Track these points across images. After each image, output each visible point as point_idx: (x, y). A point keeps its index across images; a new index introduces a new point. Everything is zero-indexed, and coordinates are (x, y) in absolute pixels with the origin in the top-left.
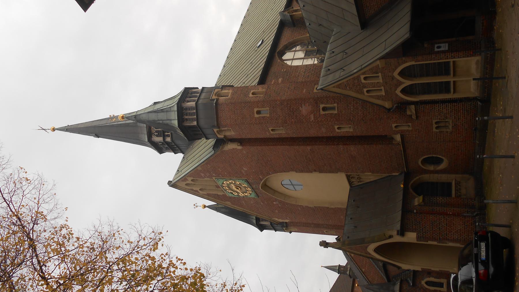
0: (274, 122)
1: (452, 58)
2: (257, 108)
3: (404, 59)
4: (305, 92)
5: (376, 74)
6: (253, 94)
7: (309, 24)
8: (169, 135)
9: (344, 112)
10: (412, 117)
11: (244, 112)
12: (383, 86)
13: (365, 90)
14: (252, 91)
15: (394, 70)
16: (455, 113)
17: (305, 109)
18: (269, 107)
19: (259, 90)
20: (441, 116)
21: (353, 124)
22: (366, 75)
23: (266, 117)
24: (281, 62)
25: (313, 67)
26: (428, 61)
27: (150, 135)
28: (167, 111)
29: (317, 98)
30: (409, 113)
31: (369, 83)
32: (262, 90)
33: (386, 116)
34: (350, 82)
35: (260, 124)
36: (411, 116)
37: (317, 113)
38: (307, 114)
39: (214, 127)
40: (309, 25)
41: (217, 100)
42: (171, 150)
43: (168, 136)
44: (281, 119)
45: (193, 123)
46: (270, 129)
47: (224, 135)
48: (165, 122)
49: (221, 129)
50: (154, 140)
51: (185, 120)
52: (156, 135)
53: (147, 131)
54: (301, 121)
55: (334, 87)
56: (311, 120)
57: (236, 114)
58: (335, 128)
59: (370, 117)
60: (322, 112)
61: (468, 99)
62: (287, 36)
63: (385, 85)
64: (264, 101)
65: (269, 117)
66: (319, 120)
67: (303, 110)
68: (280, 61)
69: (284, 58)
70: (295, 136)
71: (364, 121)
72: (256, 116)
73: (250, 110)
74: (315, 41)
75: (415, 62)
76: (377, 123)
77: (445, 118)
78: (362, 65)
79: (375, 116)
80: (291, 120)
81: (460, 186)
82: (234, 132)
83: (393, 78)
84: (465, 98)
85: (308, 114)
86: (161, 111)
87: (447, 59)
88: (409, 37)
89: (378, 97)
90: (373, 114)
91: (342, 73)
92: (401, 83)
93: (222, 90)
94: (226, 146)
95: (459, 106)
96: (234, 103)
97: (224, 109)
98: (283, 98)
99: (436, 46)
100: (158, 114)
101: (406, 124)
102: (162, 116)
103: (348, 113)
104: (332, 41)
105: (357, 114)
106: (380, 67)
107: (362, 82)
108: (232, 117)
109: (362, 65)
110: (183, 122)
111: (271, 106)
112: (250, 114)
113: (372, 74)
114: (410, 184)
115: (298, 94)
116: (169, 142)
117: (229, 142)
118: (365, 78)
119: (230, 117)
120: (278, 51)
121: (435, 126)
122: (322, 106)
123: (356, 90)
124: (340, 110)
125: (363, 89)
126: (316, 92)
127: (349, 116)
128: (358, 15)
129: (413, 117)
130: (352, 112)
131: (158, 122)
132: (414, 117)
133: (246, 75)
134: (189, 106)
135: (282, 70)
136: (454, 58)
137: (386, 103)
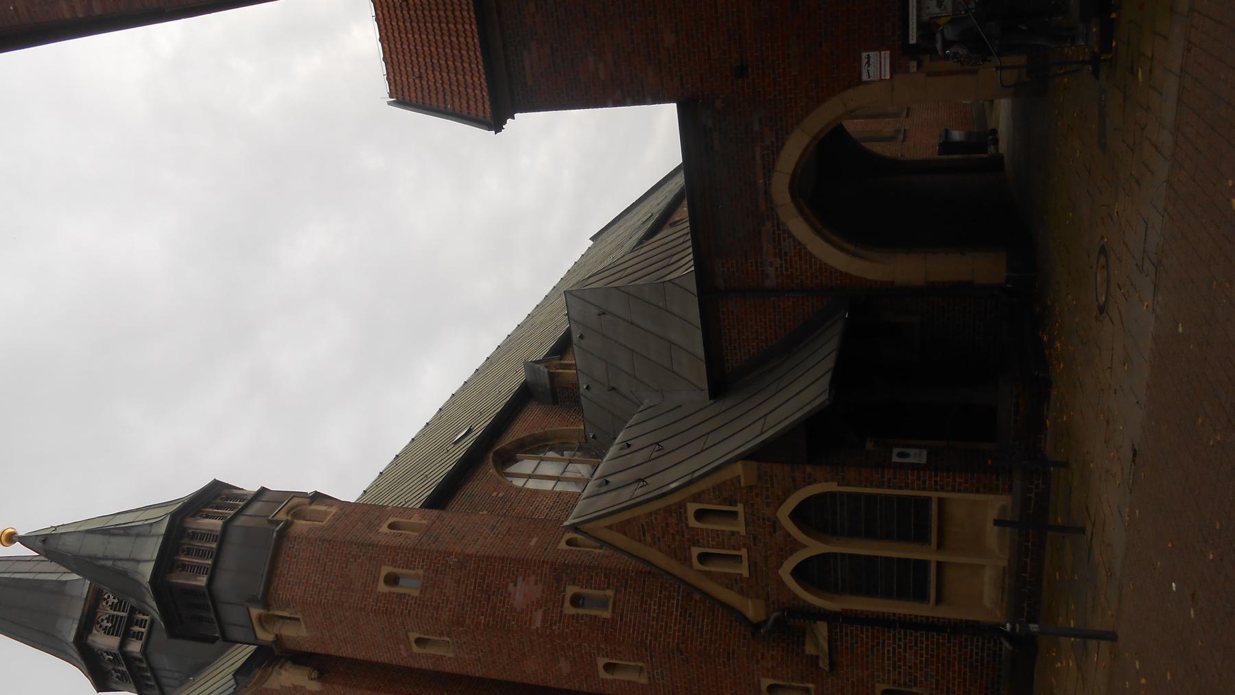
0: (427, 614)
1: (936, 490)
3: (809, 469)
4: (535, 546)
5: (731, 505)
6: (391, 526)
7: (588, 388)
8: (143, 633)
10: (817, 664)
11: (349, 571)
12: (744, 545)
13: (696, 551)
14: (391, 520)
15: (781, 501)
16: (938, 667)
17: (522, 592)
18: (424, 567)
19: (412, 520)
20: (900, 673)
21: (651, 658)
22: (701, 502)
23: (409, 595)
24: (496, 474)
26: (871, 487)
27: (88, 623)
28: (138, 535)
29: (564, 564)
30: (810, 649)
31: (707, 530)
32: (420, 522)
33: (746, 649)
34: (656, 519)
35: (386, 613)
36: (815, 659)
37: (553, 609)
38: (525, 607)
39: (253, 601)
40: (587, 391)
41: (288, 525)
42: (132, 685)
43: (138, 636)
44: (450, 611)
45: (196, 580)
46: (413, 636)
47: (276, 635)
48: (120, 564)
49: (271, 612)
50: (95, 642)
51: (178, 567)
52: (106, 627)
53: (83, 610)
54: (504, 626)
55: (610, 527)
57: (327, 575)
58: (597, 665)
60: (569, 610)
61: (974, 628)
62: (530, 423)
63: (752, 543)
64: (414, 548)
65: (416, 597)
66: (555, 630)
67: (518, 594)
68: (494, 470)
69: (514, 469)
70: (479, 672)
71: (681, 653)
72: (382, 588)
73: (369, 568)
74: (594, 437)
75: (838, 485)
76: (718, 667)
77: (910, 681)
78: (694, 472)
80: (478, 615)
82: (306, 627)
83: (775, 525)
84: (967, 621)
85: (528, 606)
86: (122, 532)
87: (924, 489)
88: (828, 403)
89: (731, 582)
91: (639, 492)
92: (796, 546)
93: (310, 504)
94: (275, 673)
95: (949, 648)
96: (331, 540)
97: (297, 554)
100: (114, 540)
101: (800, 685)
102: (119, 547)
104: (633, 423)
105: (666, 629)
106: (743, 484)
107: (690, 526)
108: (315, 580)
109: (694, 472)
110: (171, 571)
111: (432, 568)
113: (720, 504)
115: (513, 548)
116: (135, 654)
117: (289, 664)
118: (700, 515)
119: (307, 580)
120: (496, 449)
122: (571, 590)
123: (669, 546)
124: (620, 611)
125: (689, 549)
126: (563, 550)
128: (702, 327)
129: (821, 664)
130: (651, 623)
131: (103, 562)
132: (824, 664)
134: (201, 527)
135: (494, 494)
136: (942, 489)
137: (750, 602)
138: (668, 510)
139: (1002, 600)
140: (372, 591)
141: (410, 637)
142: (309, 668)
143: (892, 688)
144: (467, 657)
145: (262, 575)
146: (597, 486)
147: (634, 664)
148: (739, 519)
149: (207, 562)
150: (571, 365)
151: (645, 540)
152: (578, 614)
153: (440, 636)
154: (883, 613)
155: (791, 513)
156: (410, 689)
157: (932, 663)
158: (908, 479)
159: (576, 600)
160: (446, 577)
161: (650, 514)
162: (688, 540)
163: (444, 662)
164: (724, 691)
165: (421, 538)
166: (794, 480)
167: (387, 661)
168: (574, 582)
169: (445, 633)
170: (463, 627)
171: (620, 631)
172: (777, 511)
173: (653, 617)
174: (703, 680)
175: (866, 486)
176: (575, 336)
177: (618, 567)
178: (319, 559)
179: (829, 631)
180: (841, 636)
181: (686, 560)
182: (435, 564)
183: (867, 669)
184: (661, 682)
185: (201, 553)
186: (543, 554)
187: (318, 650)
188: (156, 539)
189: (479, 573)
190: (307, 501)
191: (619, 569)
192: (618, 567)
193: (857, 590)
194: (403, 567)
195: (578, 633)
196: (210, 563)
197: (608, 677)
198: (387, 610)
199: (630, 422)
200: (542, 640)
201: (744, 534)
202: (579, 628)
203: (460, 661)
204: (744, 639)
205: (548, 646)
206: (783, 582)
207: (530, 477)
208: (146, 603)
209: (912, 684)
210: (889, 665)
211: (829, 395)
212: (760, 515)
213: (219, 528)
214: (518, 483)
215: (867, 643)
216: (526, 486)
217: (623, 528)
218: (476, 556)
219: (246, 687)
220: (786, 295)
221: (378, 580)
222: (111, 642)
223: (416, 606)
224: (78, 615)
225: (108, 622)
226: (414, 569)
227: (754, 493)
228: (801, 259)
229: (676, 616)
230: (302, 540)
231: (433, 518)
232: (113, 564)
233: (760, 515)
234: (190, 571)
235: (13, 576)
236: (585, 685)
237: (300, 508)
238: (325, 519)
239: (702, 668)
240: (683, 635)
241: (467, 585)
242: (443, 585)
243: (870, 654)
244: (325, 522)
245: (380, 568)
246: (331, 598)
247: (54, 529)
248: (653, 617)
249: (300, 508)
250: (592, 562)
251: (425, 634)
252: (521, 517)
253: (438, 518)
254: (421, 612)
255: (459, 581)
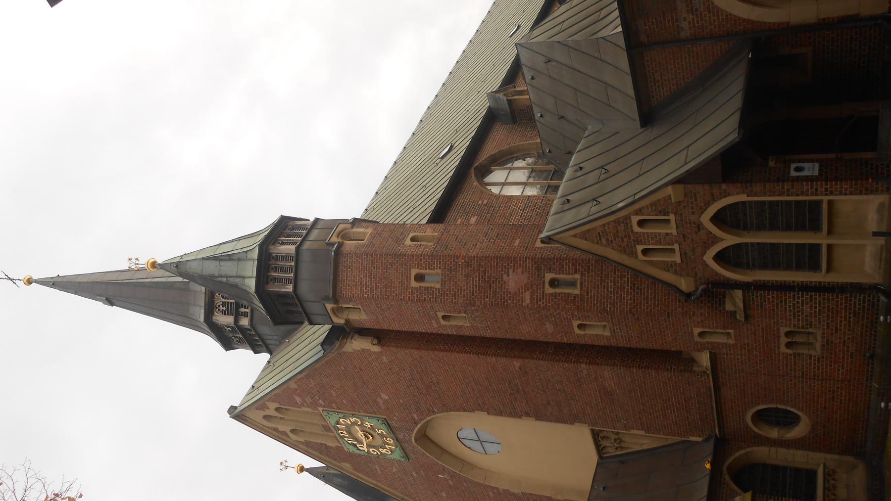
1: (826, 195)
2: (418, 268)
3: (724, 186)
4: (518, 246)
5: (664, 215)
6: (413, 239)
7: (541, 116)
8: (247, 312)
9: (594, 294)
12: (676, 242)
13: (640, 248)
14: (411, 235)
17: (513, 280)
19: (427, 234)
20: (798, 320)
21: (612, 319)
22: (642, 215)
23: (434, 288)
24: (479, 186)
25: (543, 200)
27: (210, 310)
28: (239, 260)
30: (729, 307)
31: (647, 233)
32: (432, 234)
33: (680, 309)
36: (733, 314)
39: (327, 299)
40: (533, 81)
41: (340, 245)
43: (245, 315)
45: (286, 288)
46: (440, 315)
47: (346, 320)
48: (231, 280)
51: (271, 280)
52: (223, 310)
53: (205, 300)
54: (504, 305)
55: (575, 236)
56: (524, 304)
57: (374, 278)
58: (572, 326)
59: (647, 307)
60: (549, 290)
61: (858, 288)
65: (439, 289)
66: (540, 305)
67: (511, 281)
68: (477, 183)
69: (490, 178)
72: (414, 284)
74: (550, 151)
77: (807, 324)
79: (658, 306)
80: (484, 299)
81: (834, 480)
83: (699, 227)
85: (519, 289)
86: (227, 258)
87: (817, 195)
88: (738, 140)
89: (667, 267)
90: (654, 304)
91: (594, 209)
92: (715, 240)
93: (352, 228)
94: (348, 342)
95: (837, 302)
98: (473, 253)
99: (793, 166)
102: (228, 268)
103: (601, 295)
106: (673, 201)
107: (635, 231)
108: (366, 282)
110: (267, 283)
112: (402, 280)
113: (657, 215)
114: (727, 464)
116: (246, 327)
117: (356, 336)
118: (641, 223)
121: (784, 340)
122: (549, 276)
123: (620, 246)
125: (635, 246)
127: (604, 302)
128: (631, 74)
129: (738, 317)
130: (610, 295)
131: (219, 279)
132: (740, 316)
133: (411, 209)
136: (832, 193)
137: (683, 281)
138: (617, 222)
139: (880, 267)
140: (407, 286)
141: (439, 316)
142: (371, 338)
143: (792, 330)
144: (479, 325)
145: (329, 281)
146: (561, 204)
147: (599, 324)
148: (671, 224)
149: (290, 275)
150: (523, 91)
151: (602, 243)
152: (556, 293)
153: (459, 313)
154: (785, 281)
155: (711, 219)
156: (442, 347)
157: (824, 313)
158: (804, 188)
159: (553, 283)
160: (458, 273)
161: (604, 225)
162: (634, 241)
163: (464, 329)
164: (666, 338)
165: (436, 247)
166: (712, 195)
167: (424, 331)
168: (550, 270)
169: (462, 311)
170: (474, 307)
171: (587, 303)
172: (700, 217)
173: (611, 292)
174: (650, 331)
175: (770, 196)
176: (523, 60)
177: (581, 258)
178: (366, 268)
179: (744, 295)
180: (753, 299)
181: (633, 254)
182: (448, 264)
183: (774, 318)
184: (619, 334)
185: (286, 270)
186: (525, 252)
187: (376, 327)
188: (252, 262)
189: (481, 269)
190: (349, 226)
191: (582, 259)
192: (581, 258)
193: (764, 266)
194: (426, 269)
195: (557, 306)
196: (292, 276)
197: (582, 333)
198: (419, 299)
199: (579, 147)
200: (531, 312)
201: (676, 234)
202: (558, 302)
203: (475, 328)
204: (679, 302)
205: (537, 315)
206: (707, 264)
207: (504, 184)
208: (254, 304)
209: (809, 326)
210: (790, 315)
211: (739, 134)
212: (688, 221)
213: (293, 252)
214: (495, 190)
215: (773, 302)
216: (501, 194)
217: (584, 236)
218: (477, 257)
219: (331, 352)
220: (698, 43)
221: (410, 279)
222: (227, 320)
223: (440, 295)
224: (203, 304)
225: (223, 307)
226: (434, 270)
227: (682, 206)
228: (709, 12)
229: (628, 289)
230: (352, 255)
231: (441, 230)
232: (227, 280)
233: (688, 221)
234: (280, 282)
235: (152, 281)
236: (565, 339)
237: (345, 231)
238: (365, 237)
239: (649, 324)
240: (634, 303)
241: (473, 278)
242: (456, 279)
243: (775, 308)
244: (365, 240)
245: (410, 270)
246: (379, 294)
247: (180, 257)
248: (611, 292)
249: (345, 231)
250: (562, 255)
251: (448, 313)
252: (505, 225)
253: (444, 231)
254: (444, 299)
255: (468, 275)
